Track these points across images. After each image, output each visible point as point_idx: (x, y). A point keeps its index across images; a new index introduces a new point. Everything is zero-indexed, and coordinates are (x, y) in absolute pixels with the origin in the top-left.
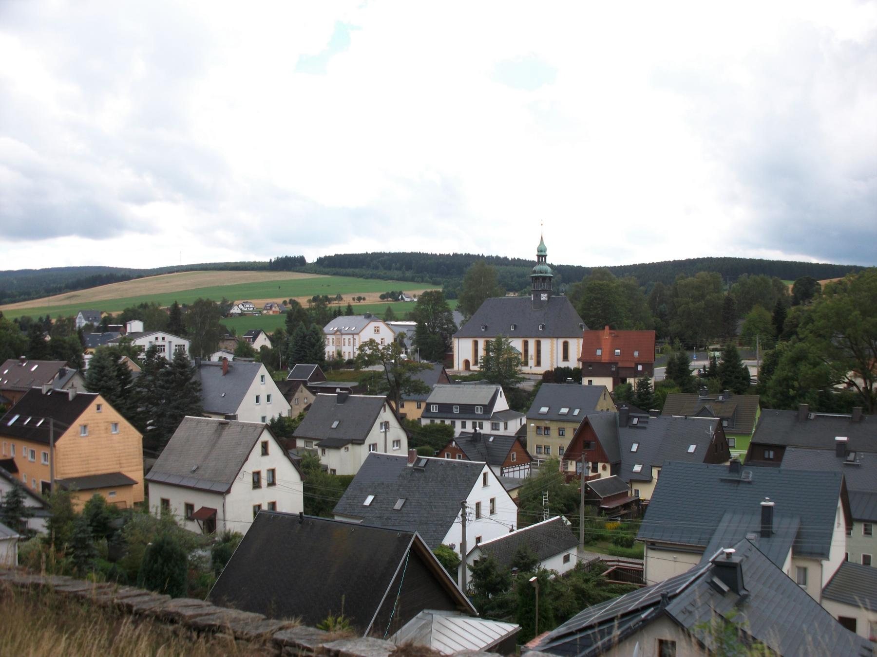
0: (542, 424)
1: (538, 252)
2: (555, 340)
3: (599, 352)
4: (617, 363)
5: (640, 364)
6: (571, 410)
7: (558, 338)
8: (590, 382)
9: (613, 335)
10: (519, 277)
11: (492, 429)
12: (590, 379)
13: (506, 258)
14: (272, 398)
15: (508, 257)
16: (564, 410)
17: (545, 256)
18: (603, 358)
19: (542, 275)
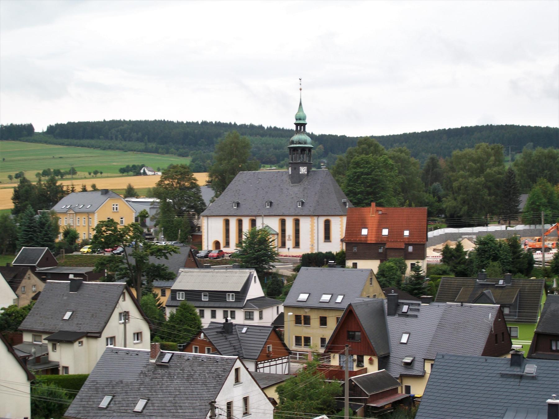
0: (302, 313)
1: (297, 120)
2: (316, 218)
3: (364, 232)
7: (318, 216)
10: (275, 148)
13: (261, 127)
15: (263, 125)
16: (326, 297)
17: (304, 125)
18: (369, 239)
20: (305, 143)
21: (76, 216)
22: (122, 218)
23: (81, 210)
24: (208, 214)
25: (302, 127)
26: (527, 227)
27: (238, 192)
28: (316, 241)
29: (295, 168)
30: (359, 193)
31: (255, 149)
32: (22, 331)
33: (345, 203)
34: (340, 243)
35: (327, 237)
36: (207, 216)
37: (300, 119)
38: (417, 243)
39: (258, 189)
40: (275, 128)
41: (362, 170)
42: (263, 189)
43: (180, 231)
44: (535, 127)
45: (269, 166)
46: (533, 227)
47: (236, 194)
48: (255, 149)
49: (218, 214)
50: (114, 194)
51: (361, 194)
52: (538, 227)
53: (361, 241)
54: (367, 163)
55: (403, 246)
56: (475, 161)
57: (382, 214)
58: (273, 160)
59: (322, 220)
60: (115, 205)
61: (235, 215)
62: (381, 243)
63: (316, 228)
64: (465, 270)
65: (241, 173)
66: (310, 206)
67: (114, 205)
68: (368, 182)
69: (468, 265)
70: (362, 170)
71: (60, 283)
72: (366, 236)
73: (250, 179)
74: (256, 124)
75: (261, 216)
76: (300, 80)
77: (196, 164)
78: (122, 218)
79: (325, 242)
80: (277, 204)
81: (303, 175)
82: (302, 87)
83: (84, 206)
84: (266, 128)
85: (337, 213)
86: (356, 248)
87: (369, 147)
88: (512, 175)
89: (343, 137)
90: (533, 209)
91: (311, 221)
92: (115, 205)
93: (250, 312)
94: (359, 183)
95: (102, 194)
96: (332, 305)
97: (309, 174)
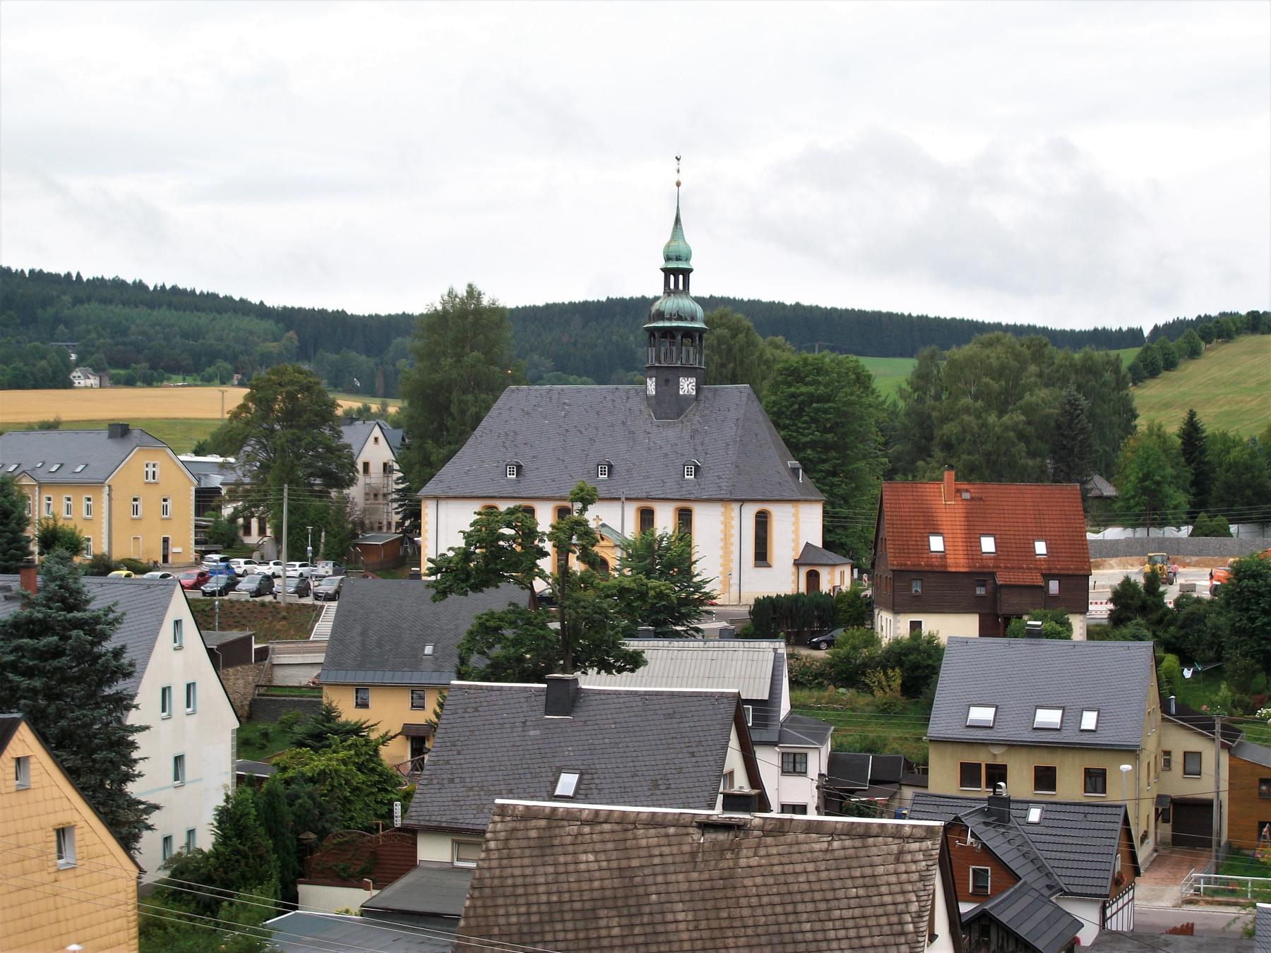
0: (982, 758)
1: (668, 259)
2: (736, 506)
3: (936, 543)
4: (993, 574)
5: (1054, 577)
6: (1071, 714)
7: (742, 501)
8: (916, 626)
9: (966, 496)
10: (185, 336)
11: (804, 773)
12: (916, 618)
13: (140, 286)
14: (200, 692)
15: (145, 282)
16: (1049, 717)
17: (686, 272)
18: (950, 561)
19: (660, 324)
20: (693, 319)
21: (40, 493)
22: (165, 500)
23: (59, 477)
24: (438, 493)
25: (681, 277)
26: (1128, 533)
27: (511, 438)
28: (735, 566)
29: (667, 381)
30: (805, 446)
31: (140, 338)
32: (410, 834)
33: (794, 471)
34: (792, 569)
35: (762, 556)
36: (437, 499)
37: (678, 259)
38: (1070, 572)
39: (567, 431)
40: (174, 288)
41: (811, 389)
42: (581, 433)
43: (323, 534)
44: (548, 306)
45: (180, 377)
46: (1141, 533)
47: (508, 444)
48: (140, 338)
49: (467, 492)
50: (146, 439)
51: (813, 449)
52: (1155, 533)
53: (932, 566)
54: (819, 370)
55: (1039, 581)
56: (1000, 373)
57: (972, 499)
58: (184, 363)
59: (750, 511)
60: (151, 466)
61: (516, 495)
62: (981, 574)
63: (735, 532)
64: (1177, 638)
65: (513, 391)
66: (719, 477)
67: (154, 466)
68: (827, 420)
69: (1182, 627)
70: (811, 389)
71: (501, 689)
72: (943, 555)
73: (539, 405)
74: (109, 276)
75: (619, 499)
76: (678, 159)
77: (15, 369)
78: (135, 500)
79: (756, 566)
80: (627, 471)
81: (686, 398)
82: (682, 178)
83: (63, 468)
84: (151, 288)
85: (786, 496)
86: (919, 583)
87: (734, 336)
88: (1076, 410)
89: (340, 316)
90: (1145, 491)
91: (723, 514)
92: (151, 466)
93: (795, 754)
94: (805, 422)
95: (111, 437)
96: (1069, 736)
97: (702, 397)
